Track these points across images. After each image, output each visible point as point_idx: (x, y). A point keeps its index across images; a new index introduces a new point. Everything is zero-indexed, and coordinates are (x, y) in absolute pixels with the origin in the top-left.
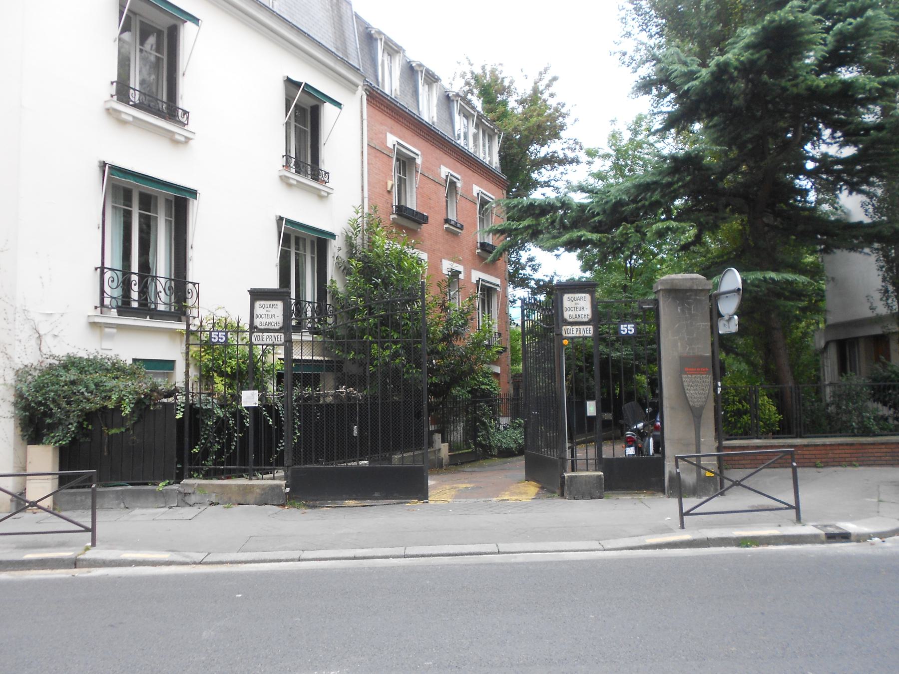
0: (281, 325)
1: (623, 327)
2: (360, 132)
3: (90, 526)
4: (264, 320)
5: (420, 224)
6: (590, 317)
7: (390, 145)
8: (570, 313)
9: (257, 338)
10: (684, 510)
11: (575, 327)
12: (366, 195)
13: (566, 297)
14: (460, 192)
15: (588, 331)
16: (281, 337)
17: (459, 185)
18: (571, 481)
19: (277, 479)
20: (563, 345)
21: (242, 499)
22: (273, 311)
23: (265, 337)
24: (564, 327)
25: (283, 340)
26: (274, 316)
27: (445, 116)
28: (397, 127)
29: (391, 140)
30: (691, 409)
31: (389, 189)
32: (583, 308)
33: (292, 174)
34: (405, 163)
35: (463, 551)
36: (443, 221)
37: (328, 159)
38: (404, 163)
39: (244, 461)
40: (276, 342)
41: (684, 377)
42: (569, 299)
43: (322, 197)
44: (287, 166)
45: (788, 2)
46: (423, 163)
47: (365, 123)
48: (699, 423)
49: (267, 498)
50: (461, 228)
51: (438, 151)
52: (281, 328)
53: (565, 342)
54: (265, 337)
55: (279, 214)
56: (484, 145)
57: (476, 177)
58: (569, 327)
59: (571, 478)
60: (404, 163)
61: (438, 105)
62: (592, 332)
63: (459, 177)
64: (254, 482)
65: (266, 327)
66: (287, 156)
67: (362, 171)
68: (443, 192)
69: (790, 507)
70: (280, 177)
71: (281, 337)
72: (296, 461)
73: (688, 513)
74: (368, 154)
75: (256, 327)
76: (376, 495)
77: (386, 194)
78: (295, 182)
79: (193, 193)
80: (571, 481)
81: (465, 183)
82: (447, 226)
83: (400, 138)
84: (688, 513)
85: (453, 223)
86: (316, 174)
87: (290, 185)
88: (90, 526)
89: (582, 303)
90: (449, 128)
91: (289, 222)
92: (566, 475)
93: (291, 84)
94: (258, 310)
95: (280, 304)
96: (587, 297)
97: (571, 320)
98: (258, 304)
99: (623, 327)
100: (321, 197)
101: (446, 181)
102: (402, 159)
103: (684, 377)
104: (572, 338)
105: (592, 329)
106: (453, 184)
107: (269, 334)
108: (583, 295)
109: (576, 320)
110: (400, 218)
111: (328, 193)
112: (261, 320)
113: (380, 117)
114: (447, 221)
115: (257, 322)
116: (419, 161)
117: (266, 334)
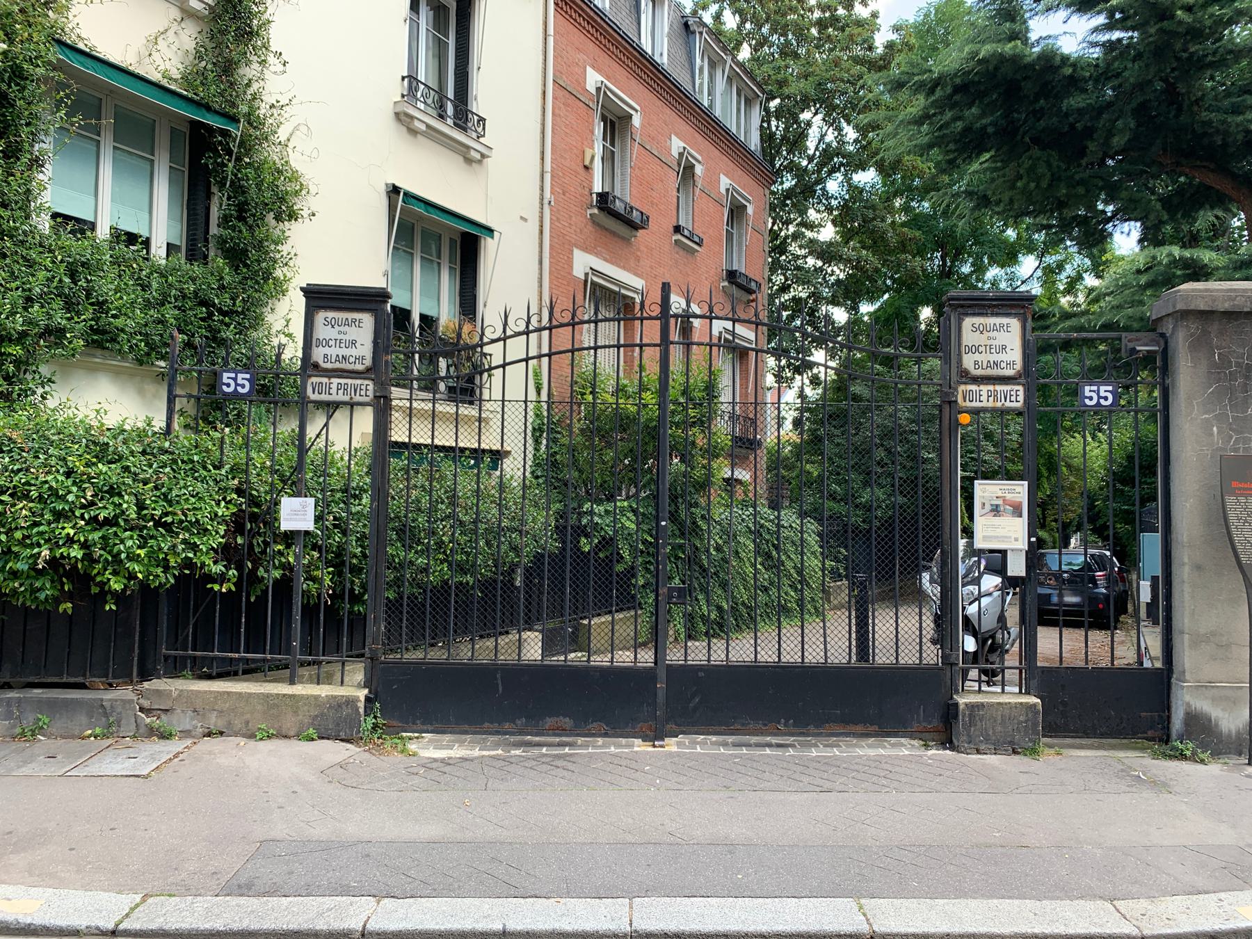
0: (368, 362)
2: (541, 58)
4: (333, 351)
7: (591, 87)
9: (317, 388)
11: (985, 389)
12: (548, 167)
13: (968, 322)
14: (699, 183)
15: (1015, 397)
16: (368, 388)
17: (699, 169)
19: (350, 685)
20: (958, 424)
21: (272, 725)
22: (352, 333)
23: (334, 386)
24: (962, 388)
25: (370, 393)
26: (354, 343)
27: (681, 56)
28: (604, 59)
29: (593, 79)
31: (587, 163)
32: (1004, 348)
33: (423, 115)
34: (616, 124)
36: (672, 229)
37: (485, 94)
38: (613, 123)
39: (282, 645)
40: (357, 398)
42: (975, 329)
43: (471, 159)
44: (411, 92)
45: (1099, 3)
46: (642, 125)
47: (551, 40)
49: (334, 725)
51: (668, 111)
52: (368, 370)
54: (334, 386)
55: (391, 181)
56: (738, 110)
57: (725, 162)
58: (974, 387)
59: (972, 707)
60: (613, 123)
61: (669, 35)
62: (1021, 398)
63: (700, 158)
64: (298, 689)
65: (337, 365)
66: (412, 78)
67: (541, 218)
68: (673, 181)
70: (397, 114)
71: (368, 388)
72: (393, 640)
74: (555, 98)
75: (316, 366)
76: (550, 722)
77: (582, 171)
78: (423, 127)
81: (707, 170)
82: (678, 237)
83: (608, 78)
85: (686, 233)
86: (463, 117)
87: (413, 132)
89: (1001, 338)
90: (688, 77)
92: (962, 700)
93: (471, 159)
94: (321, 331)
95: (367, 320)
97: (979, 372)
98: (321, 316)
100: (469, 161)
101: (679, 165)
102: (609, 116)
103: (1230, 500)
105: (1021, 393)
106: (688, 171)
107: (343, 381)
108: (1005, 320)
109: (989, 372)
111: (483, 156)
112: (327, 350)
113: (577, 37)
114: (677, 229)
115: (318, 354)
116: (636, 121)
117: (335, 381)
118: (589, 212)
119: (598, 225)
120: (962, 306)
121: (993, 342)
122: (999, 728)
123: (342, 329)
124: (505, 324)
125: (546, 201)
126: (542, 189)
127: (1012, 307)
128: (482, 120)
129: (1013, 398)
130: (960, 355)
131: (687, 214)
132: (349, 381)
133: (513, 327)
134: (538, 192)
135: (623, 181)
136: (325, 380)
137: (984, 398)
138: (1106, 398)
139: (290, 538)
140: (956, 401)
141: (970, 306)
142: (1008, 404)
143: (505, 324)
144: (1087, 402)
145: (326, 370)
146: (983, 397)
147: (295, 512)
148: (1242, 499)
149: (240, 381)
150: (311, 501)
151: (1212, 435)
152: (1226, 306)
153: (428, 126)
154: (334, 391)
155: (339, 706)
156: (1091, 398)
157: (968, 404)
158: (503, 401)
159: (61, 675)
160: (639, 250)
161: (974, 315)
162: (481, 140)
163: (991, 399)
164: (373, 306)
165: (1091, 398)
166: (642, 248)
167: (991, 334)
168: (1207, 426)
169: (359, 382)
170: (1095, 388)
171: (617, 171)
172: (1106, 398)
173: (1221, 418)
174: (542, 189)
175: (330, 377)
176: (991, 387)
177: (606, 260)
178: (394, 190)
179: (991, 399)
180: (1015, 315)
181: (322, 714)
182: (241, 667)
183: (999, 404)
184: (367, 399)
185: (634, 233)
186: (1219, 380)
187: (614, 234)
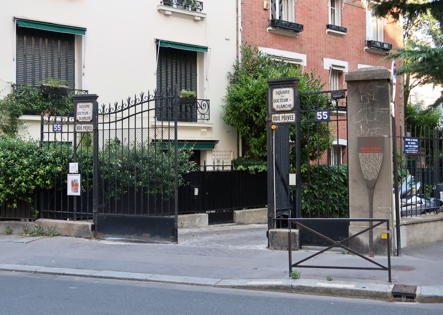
1: (318, 114)
3: (386, 266)
5: (298, 32)
6: (292, 106)
8: (278, 104)
9: (79, 128)
10: (293, 263)
11: (281, 115)
15: (292, 118)
18: (273, 236)
24: (273, 115)
26: (87, 113)
30: (367, 181)
31: (265, 7)
35: (59, 272)
41: (360, 154)
42: (277, 93)
48: (373, 195)
50: (345, 30)
52: (91, 121)
53: (274, 127)
58: (277, 115)
62: (294, 118)
65: (83, 120)
69: (384, 268)
70: (159, 10)
73: (295, 265)
75: (78, 121)
77: (264, 12)
79: (83, 30)
80: (273, 236)
82: (329, 30)
84: (295, 265)
88: (386, 266)
91: (162, 42)
96: (291, 90)
99: (318, 114)
104: (280, 124)
105: (294, 117)
107: (85, 125)
110: (274, 29)
117: (83, 125)
118: (268, 29)
119: (274, 34)
120: (273, 85)
121: (283, 98)
122: (282, 241)
123: (84, 108)
124: (129, 103)
125: (239, 30)
126: (237, 24)
127: (290, 83)
128: (201, 3)
129: (291, 118)
130: (272, 103)
131: (338, 17)
132: (86, 125)
133: (138, 102)
134: (236, 26)
135: (291, 10)
136: (80, 125)
137: (281, 119)
138: (325, 117)
139: (294, 172)
140: (271, 121)
141: (275, 85)
142: (289, 121)
143: (129, 103)
144: (318, 118)
145: (80, 122)
146: (280, 119)
147: (73, 167)
148: (365, 154)
149: (58, 127)
150: (77, 164)
151: (360, 129)
152: (364, 78)
153: (172, 12)
154: (82, 129)
155: (84, 227)
156: (319, 117)
157: (275, 121)
158: (129, 129)
159: (15, 217)
160: (302, 41)
161: (277, 88)
162: (202, 11)
163: (283, 119)
164: (92, 100)
165: (319, 117)
166: (304, 39)
167: (283, 95)
168: (358, 126)
169: (89, 125)
170: (321, 113)
171: (289, 5)
172: (325, 117)
173: (363, 123)
174: (237, 24)
175: (81, 124)
176: (283, 115)
177: (279, 49)
178: (157, 41)
179: (283, 119)
180: (292, 87)
181: (80, 230)
182: (88, 217)
183: (286, 121)
184: (91, 131)
185: (297, 34)
186: (363, 107)
187: (285, 36)
